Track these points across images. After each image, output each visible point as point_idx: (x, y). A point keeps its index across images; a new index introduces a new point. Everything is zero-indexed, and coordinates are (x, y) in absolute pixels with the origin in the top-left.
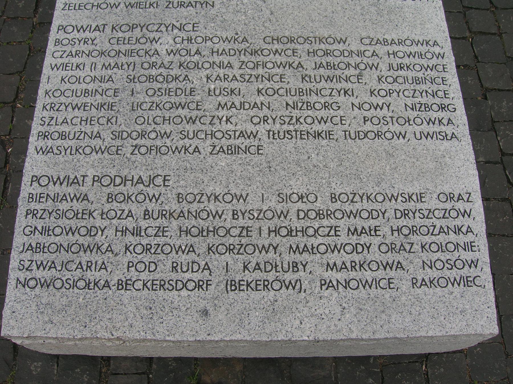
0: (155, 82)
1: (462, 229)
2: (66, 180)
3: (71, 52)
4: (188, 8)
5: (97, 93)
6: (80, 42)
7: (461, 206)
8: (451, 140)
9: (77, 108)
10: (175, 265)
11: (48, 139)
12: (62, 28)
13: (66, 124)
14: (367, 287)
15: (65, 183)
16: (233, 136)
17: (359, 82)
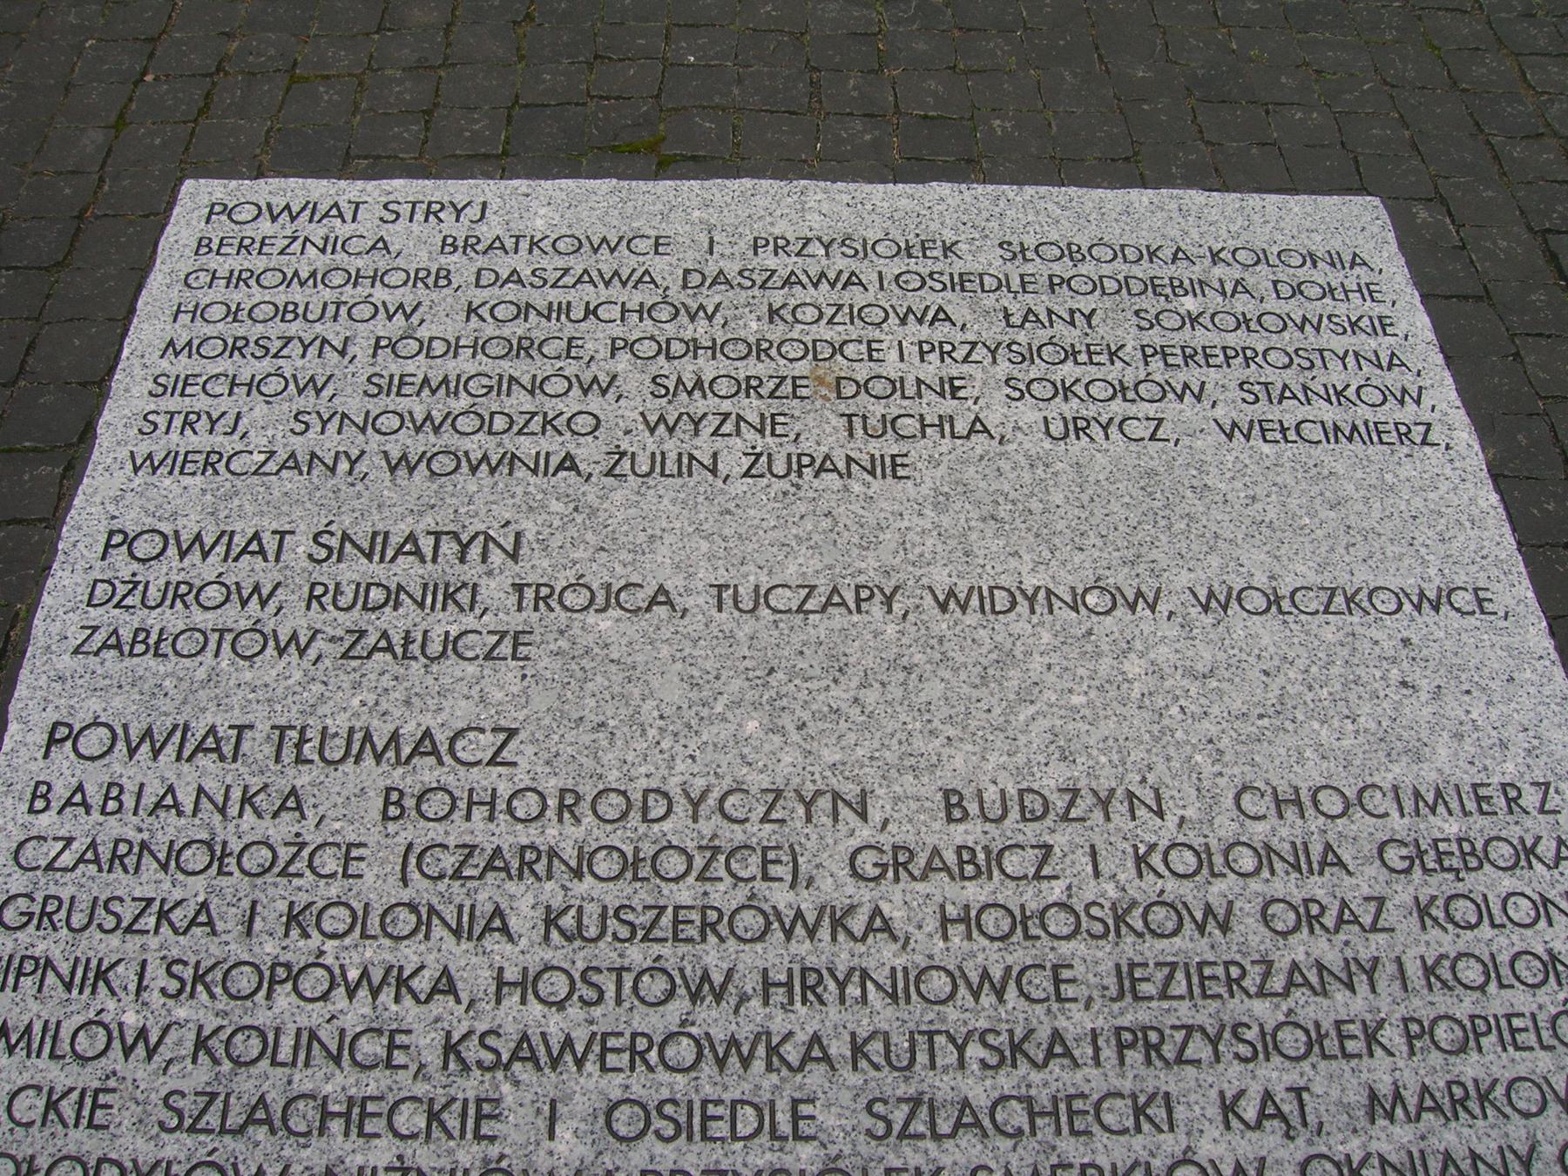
0: (742, 377)
6: (324, 423)
8: (968, 437)
9: (145, 748)
10: (319, 591)
12: (119, 540)
13: (82, 810)
15: (170, 749)
16: (610, 993)
17: (1060, 999)
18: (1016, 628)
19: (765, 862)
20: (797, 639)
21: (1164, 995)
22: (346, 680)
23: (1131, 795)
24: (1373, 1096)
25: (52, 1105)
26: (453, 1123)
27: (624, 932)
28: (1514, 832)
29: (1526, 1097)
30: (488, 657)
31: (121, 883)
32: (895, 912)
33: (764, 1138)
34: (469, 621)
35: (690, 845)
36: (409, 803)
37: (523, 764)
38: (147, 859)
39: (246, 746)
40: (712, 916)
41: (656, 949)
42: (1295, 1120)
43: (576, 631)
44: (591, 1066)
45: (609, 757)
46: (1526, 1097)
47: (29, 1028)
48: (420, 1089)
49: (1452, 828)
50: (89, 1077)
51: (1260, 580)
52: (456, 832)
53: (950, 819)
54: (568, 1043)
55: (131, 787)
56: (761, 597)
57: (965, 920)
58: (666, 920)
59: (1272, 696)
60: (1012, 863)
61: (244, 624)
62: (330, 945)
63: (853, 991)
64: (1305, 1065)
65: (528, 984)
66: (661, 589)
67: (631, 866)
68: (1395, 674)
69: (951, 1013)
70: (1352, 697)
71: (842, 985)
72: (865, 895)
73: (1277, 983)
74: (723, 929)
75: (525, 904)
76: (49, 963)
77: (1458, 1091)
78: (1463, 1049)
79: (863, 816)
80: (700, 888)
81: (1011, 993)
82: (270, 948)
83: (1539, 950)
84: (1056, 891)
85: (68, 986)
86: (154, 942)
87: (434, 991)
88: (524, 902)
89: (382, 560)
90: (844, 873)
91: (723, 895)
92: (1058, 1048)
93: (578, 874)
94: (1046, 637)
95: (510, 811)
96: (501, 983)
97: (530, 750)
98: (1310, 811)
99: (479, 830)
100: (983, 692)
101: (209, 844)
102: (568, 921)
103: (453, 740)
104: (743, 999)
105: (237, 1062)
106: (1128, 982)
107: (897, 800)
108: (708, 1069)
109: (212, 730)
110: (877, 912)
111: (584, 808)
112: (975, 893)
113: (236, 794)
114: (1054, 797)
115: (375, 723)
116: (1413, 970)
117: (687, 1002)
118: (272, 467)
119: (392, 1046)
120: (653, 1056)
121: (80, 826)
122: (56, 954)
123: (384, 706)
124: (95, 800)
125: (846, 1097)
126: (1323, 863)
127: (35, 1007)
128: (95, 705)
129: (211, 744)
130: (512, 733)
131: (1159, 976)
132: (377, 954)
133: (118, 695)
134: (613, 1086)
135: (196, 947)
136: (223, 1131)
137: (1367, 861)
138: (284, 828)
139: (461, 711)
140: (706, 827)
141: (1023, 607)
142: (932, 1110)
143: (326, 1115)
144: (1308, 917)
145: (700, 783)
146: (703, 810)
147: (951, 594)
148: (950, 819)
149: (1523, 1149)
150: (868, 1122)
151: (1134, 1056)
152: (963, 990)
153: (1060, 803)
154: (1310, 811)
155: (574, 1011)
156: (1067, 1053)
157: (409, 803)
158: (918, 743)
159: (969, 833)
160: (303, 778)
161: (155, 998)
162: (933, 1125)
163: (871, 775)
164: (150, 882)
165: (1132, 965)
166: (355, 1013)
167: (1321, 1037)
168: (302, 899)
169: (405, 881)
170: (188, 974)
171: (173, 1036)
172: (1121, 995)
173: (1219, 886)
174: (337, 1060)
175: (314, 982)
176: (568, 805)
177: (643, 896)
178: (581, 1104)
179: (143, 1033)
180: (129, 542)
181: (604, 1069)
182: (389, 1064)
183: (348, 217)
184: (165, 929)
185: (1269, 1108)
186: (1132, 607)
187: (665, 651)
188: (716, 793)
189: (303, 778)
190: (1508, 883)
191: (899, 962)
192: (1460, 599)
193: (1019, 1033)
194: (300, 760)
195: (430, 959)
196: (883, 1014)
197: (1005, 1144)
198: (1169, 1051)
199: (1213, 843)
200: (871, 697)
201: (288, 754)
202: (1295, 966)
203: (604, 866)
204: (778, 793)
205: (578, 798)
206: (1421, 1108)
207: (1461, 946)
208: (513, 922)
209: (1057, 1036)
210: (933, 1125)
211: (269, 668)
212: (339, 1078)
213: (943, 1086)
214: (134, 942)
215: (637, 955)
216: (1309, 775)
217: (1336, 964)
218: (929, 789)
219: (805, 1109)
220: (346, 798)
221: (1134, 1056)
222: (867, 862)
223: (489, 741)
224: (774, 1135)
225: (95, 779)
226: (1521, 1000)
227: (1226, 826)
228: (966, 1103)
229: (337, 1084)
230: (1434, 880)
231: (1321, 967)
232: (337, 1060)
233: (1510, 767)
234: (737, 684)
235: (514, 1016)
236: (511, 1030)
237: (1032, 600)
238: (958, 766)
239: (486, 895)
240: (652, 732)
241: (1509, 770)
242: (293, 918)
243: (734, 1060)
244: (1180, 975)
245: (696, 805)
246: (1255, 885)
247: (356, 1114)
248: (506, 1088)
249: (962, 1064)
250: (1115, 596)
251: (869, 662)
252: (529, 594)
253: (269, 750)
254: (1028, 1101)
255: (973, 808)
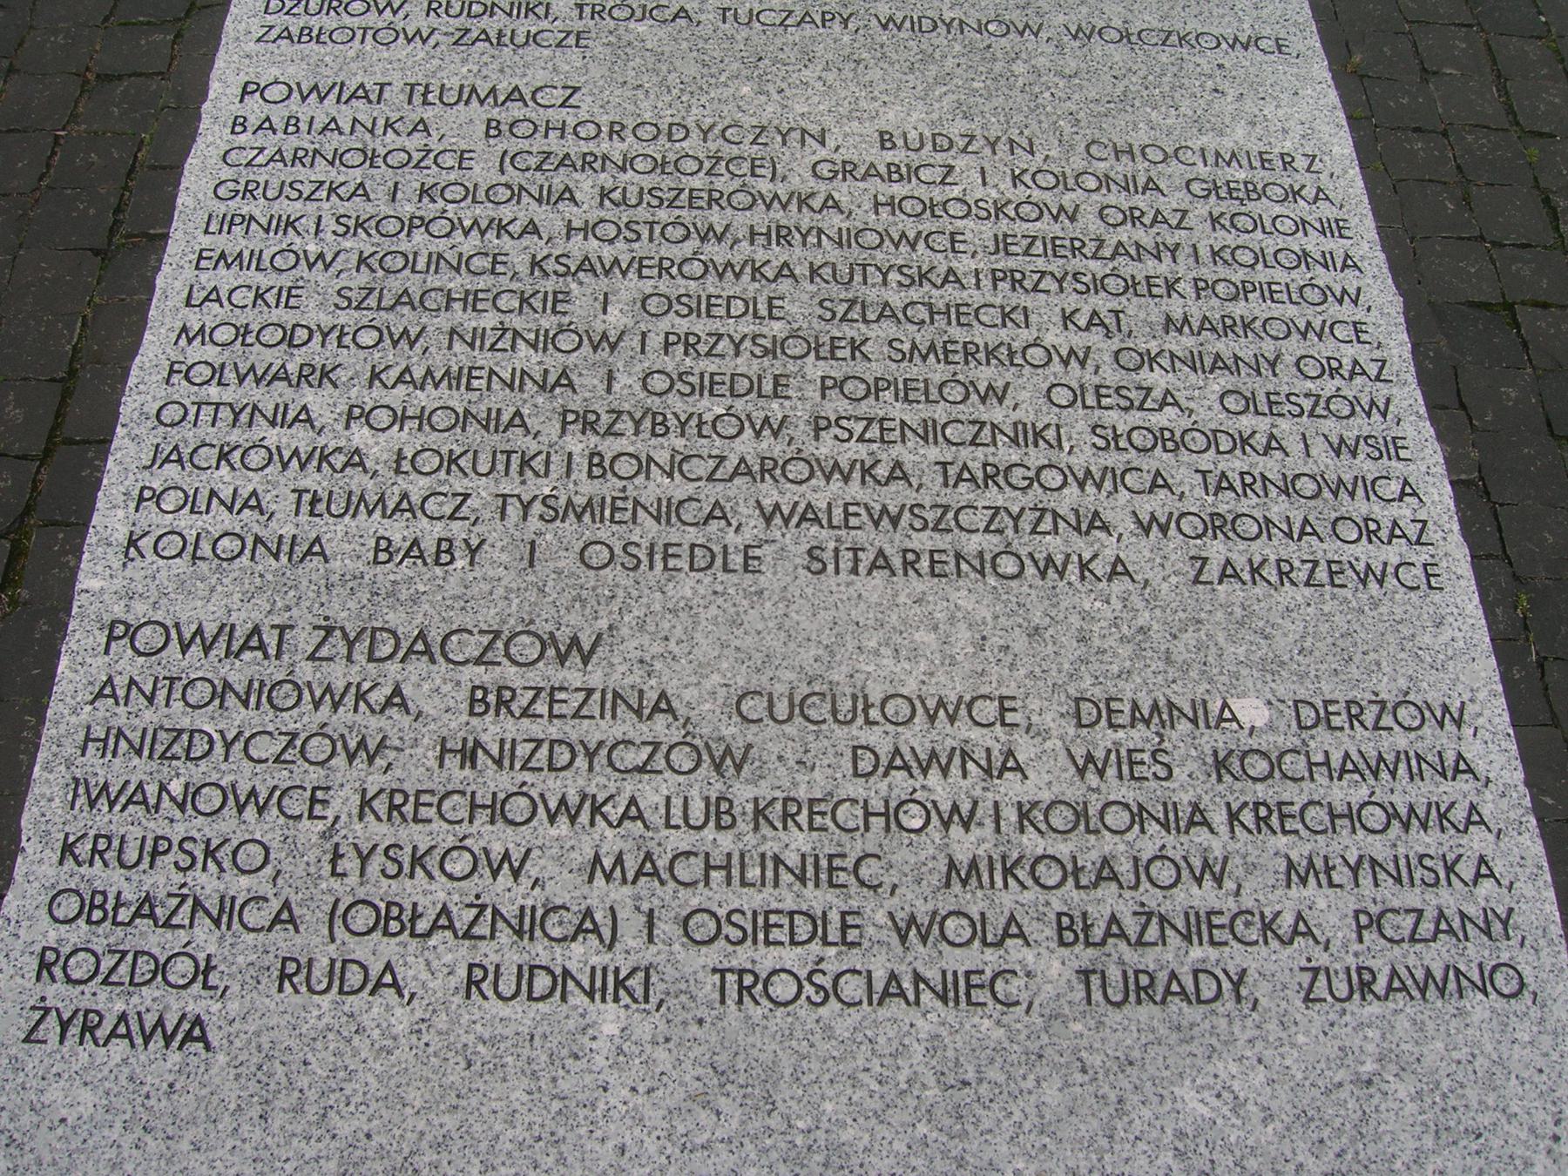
1: (1450, 816)
2: (224, 638)
3: (280, 151)
4: (561, 206)
5: (261, 549)
7: (1433, 739)
9: (320, 265)
11: (106, 864)
12: (120, 632)
14: (1432, 992)
18: (936, 42)
19: (753, 167)
20: (779, 42)
21: (1026, 253)
22: (457, 59)
23: (1011, 141)
24: (1169, 319)
25: (259, 296)
26: (537, 304)
27: (655, 202)
28: (1286, 182)
29: (1277, 329)
30: (559, 45)
31: (300, 172)
32: (842, 197)
33: (749, 317)
34: (545, 24)
35: (701, 156)
36: (505, 128)
37: (584, 107)
38: (318, 159)
39: (386, 95)
40: (716, 195)
41: (677, 212)
42: (1113, 328)
43: (621, 31)
44: (632, 275)
45: (645, 104)
46: (1277, 329)
47: (240, 254)
48: (515, 286)
49: (1242, 175)
50: (286, 280)
51: (1117, 23)
52: (538, 144)
53: (883, 148)
54: (616, 262)
55: (304, 119)
56: (754, 16)
57: (891, 204)
58: (685, 196)
59: (1119, 91)
60: (925, 174)
61: (380, 25)
62: (450, 207)
63: (812, 239)
64: (1123, 299)
65: (588, 230)
66: (682, 9)
67: (660, 166)
68: (1210, 83)
69: (879, 255)
70: (1177, 95)
71: (804, 237)
72: (823, 187)
73: (1107, 252)
74: (724, 203)
75: (586, 186)
76: (252, 218)
77: (1229, 322)
78: (1235, 298)
79: (823, 143)
80: (708, 179)
81: (921, 246)
82: (408, 209)
83: (1296, 249)
84: (956, 191)
85: (267, 231)
86: (326, 205)
87: (524, 232)
88: (586, 185)
89: (150, 757)
90: (808, 175)
91: (723, 183)
92: (951, 277)
93: (623, 169)
94: (958, 48)
95: (576, 133)
96: (570, 228)
97: (589, 99)
98: (1139, 158)
99: (553, 142)
100: (911, 77)
101: (363, 151)
102: (616, 195)
103: (534, 94)
104: (736, 241)
105: (388, 271)
106: (1002, 244)
107: (846, 135)
108: (711, 278)
109: (362, 86)
110: (830, 197)
111: (628, 132)
112: (898, 190)
113: (381, 122)
114: (956, 139)
115: (479, 82)
116: (1204, 252)
117: (697, 243)
118: (261, 159)
119: (495, 262)
120: (674, 270)
121: (271, 142)
122: (257, 213)
123: (485, 72)
124: (279, 126)
125: (805, 297)
126: (1145, 189)
127: (244, 242)
128: (275, 72)
129: (361, 93)
130: (576, 90)
131: (1025, 242)
132: (484, 212)
133: (291, 65)
134: (648, 286)
135: (357, 207)
136: (379, 308)
137: (1177, 189)
138: (418, 140)
139: (541, 77)
140: (713, 146)
141: (942, 29)
142: (863, 307)
143: (450, 300)
144: (1132, 217)
145: (708, 121)
146: (710, 136)
147: (891, 19)
148: (883, 148)
149: (1271, 357)
150: (820, 311)
151: (1004, 286)
152: (887, 242)
153: (961, 143)
154: (1139, 158)
155: (620, 245)
156: (958, 281)
157: (505, 128)
158: (863, 104)
159: (898, 156)
160: (428, 113)
161: (330, 237)
162: (864, 315)
163: (828, 121)
164: (322, 171)
165: (1006, 236)
166: (470, 244)
167: (1135, 284)
168: (430, 181)
169: (502, 171)
170: (352, 223)
171: (342, 257)
172: (997, 251)
173: (1069, 196)
174: (457, 270)
175: (440, 227)
176: (616, 130)
177: (668, 182)
178: (624, 295)
179: (321, 256)
180: (131, 633)
181: (641, 277)
182: (493, 272)
183: (272, 651)
184: (333, 198)
185: (1095, 319)
186: (1022, 34)
187: (685, 45)
188: (720, 127)
189: (428, 113)
190: (1278, 209)
191: (844, 225)
192: (1263, 44)
193: (925, 268)
194: (425, 103)
195: (521, 214)
196: (832, 253)
197: (912, 328)
198: (1028, 284)
199: (1068, 171)
200: (830, 77)
201: (417, 99)
202: (1120, 243)
203: (640, 165)
204: (763, 128)
205: (623, 127)
206: (1201, 328)
207: (1240, 242)
208: (578, 196)
209: (950, 271)
210: (864, 315)
211: (401, 50)
212: (459, 280)
213: (872, 294)
214: (311, 207)
215: (663, 215)
216: (1141, 137)
217: (1150, 246)
218: (870, 129)
219: (777, 303)
220: (460, 126)
221: (1004, 286)
222: (824, 170)
223: (559, 95)
224: (755, 315)
225: (278, 116)
226: (1280, 275)
227: (1078, 163)
228: (887, 304)
229: (458, 283)
230: (1224, 204)
231: (1138, 246)
232: (457, 270)
233: (1288, 144)
234: (735, 66)
235: (578, 247)
236: (578, 255)
237: (949, 26)
238: (890, 118)
239: (559, 180)
240: (675, 92)
241: (1288, 146)
242: (424, 192)
243: (729, 274)
244: (1039, 243)
245: (705, 133)
246: (1095, 197)
247: (471, 300)
248: (573, 286)
249: (885, 282)
250: (1009, 27)
251: (830, 56)
252: (587, 10)
253: (404, 97)
254: (930, 306)
255: (900, 143)
